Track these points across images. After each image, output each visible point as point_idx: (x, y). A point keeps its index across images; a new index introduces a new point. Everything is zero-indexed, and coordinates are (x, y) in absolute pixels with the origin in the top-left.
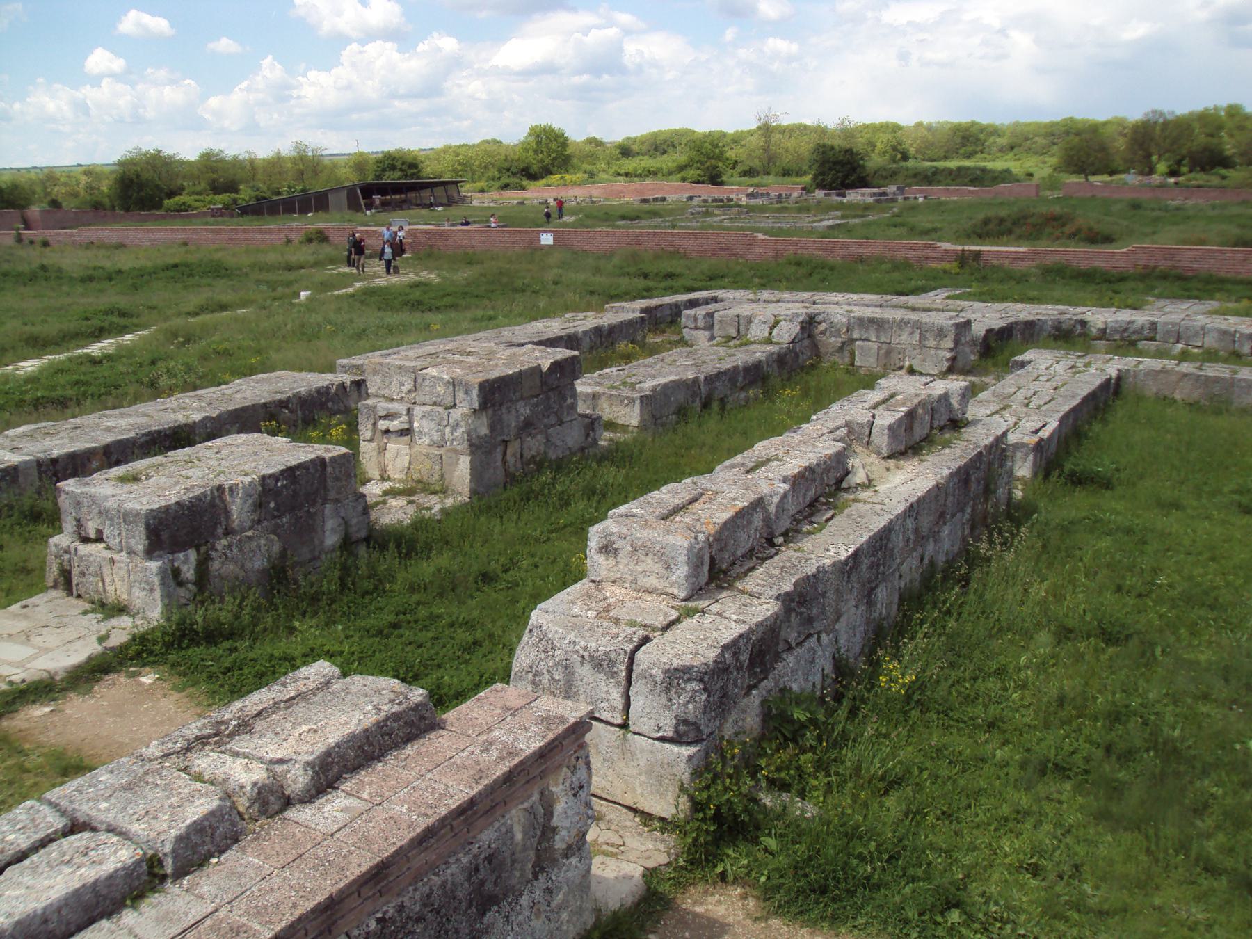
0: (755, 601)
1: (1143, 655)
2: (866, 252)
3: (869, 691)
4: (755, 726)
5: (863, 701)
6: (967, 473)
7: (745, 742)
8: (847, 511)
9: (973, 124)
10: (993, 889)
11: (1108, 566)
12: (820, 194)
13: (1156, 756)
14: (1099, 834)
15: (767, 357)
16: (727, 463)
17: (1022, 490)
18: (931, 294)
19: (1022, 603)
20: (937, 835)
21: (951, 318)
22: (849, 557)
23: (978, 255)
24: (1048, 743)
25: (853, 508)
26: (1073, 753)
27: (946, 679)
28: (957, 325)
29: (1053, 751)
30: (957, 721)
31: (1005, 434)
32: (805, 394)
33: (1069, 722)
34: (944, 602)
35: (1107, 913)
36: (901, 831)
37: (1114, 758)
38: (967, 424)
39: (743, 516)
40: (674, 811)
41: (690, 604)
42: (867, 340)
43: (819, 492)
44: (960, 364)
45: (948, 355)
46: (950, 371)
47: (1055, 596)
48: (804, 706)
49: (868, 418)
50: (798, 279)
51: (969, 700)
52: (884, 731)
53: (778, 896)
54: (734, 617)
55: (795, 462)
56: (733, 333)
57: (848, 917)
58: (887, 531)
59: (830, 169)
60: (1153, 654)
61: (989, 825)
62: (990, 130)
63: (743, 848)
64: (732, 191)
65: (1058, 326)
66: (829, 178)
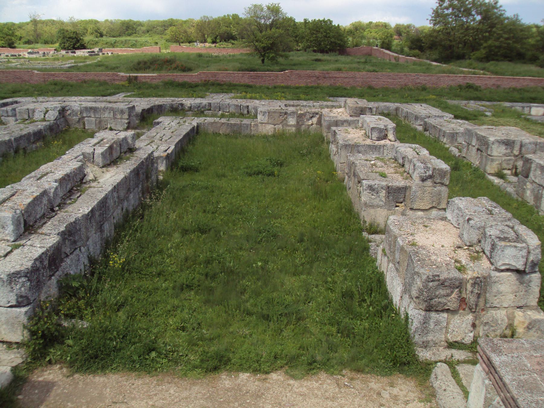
0: (48, 237)
1: (216, 235)
2: (87, 78)
3: (106, 269)
4: (56, 293)
5: (104, 273)
6: (138, 170)
7: (51, 301)
8: (86, 192)
9: (131, 21)
10: (168, 340)
11: (200, 203)
12: (63, 52)
13: (224, 275)
14: (206, 309)
16: (27, 176)
18: (117, 95)
19: (166, 222)
20: (141, 323)
21: (126, 105)
22: (89, 212)
23: (136, 78)
24: (183, 278)
25: (89, 190)
26: (193, 279)
27: (138, 258)
28: (129, 108)
29: (185, 280)
30: (145, 275)
31: (152, 153)
32: (64, 143)
33: (190, 267)
34: (134, 226)
35: (213, 339)
36: (127, 324)
37: (209, 278)
38: (136, 149)
40: (22, 338)
41: (17, 243)
42: (90, 117)
43: (73, 185)
44: (132, 124)
45: (126, 121)
46: (128, 128)
47: (180, 217)
48: (77, 280)
49: (92, 150)
50: (56, 91)
51: (150, 265)
52: (114, 284)
53: (76, 364)
54: (39, 246)
55: (60, 173)
56: (26, 117)
57: (108, 366)
58: (105, 198)
59: (67, 41)
60: (220, 236)
61: (163, 314)
62: (138, 23)
63: (57, 346)
64: (20, 51)
65: (172, 106)
66: (67, 45)
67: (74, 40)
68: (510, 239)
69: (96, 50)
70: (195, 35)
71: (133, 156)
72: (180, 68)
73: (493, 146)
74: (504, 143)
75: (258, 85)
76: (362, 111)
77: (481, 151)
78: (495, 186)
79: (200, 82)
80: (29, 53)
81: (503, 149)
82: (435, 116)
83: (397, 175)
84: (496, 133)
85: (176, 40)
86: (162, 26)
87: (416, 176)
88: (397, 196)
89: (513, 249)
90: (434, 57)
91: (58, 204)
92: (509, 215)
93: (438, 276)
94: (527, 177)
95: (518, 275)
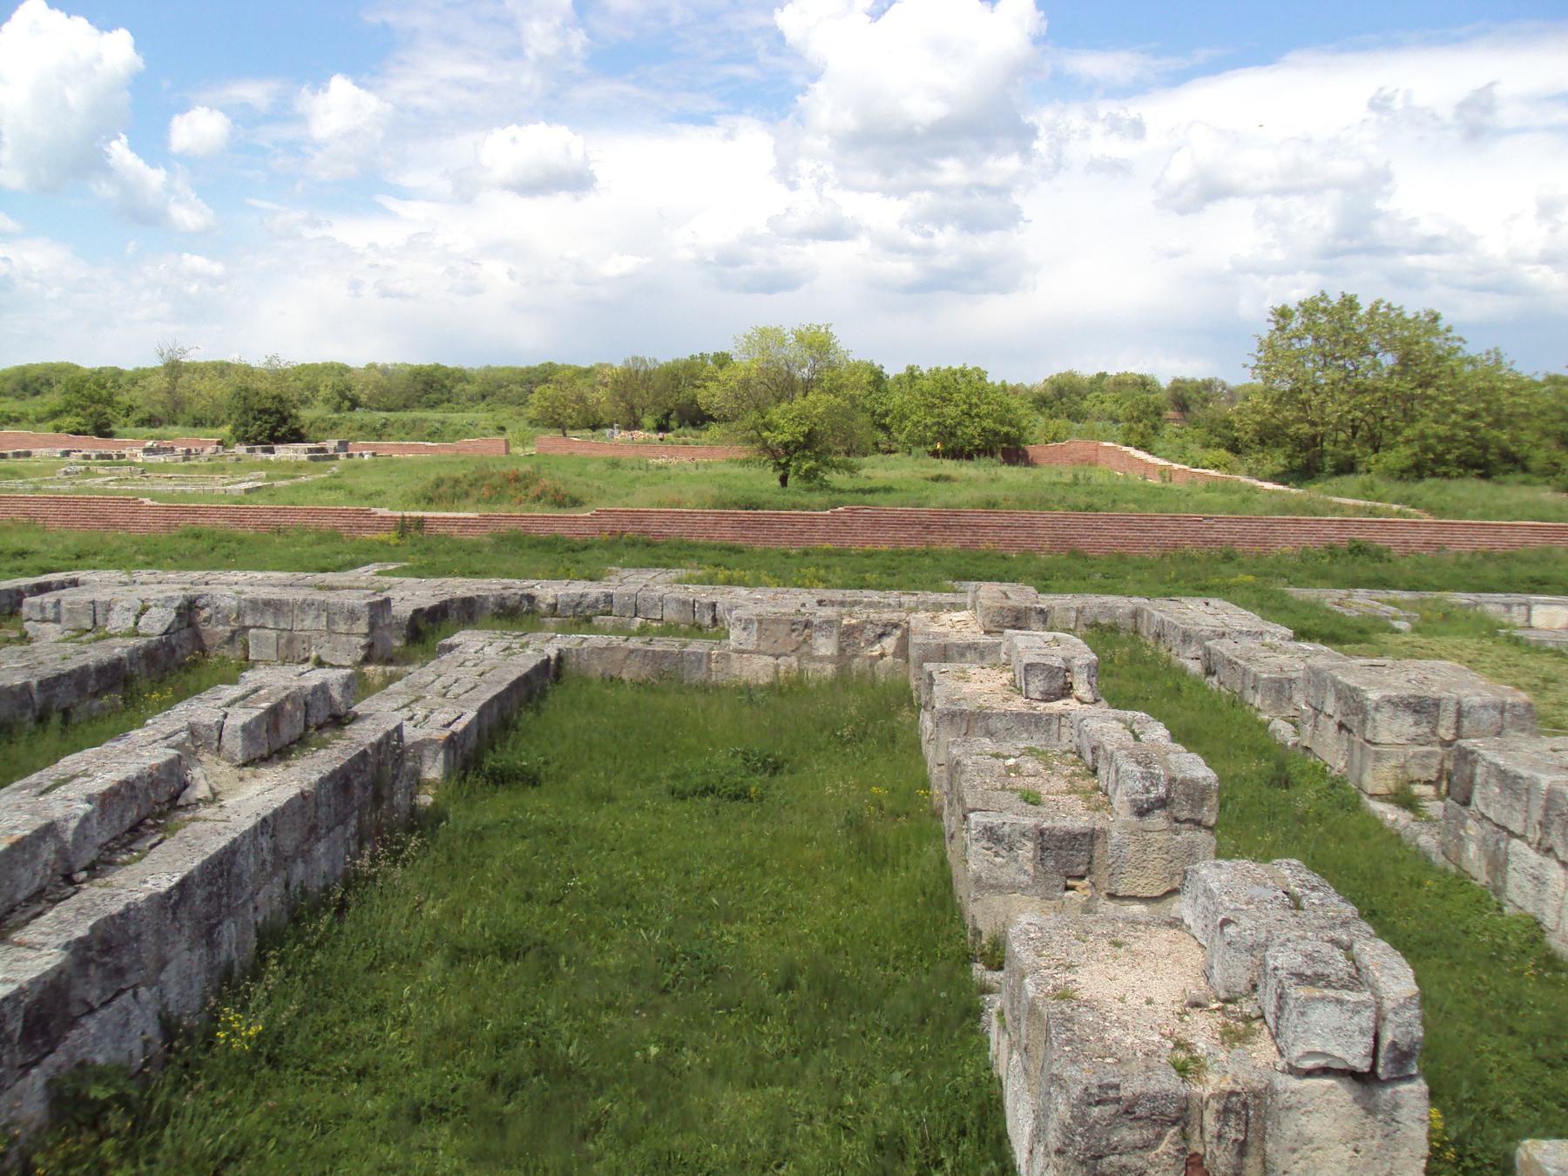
0: (32, 954)
6: (347, 779)
8: (180, 833)
9: (437, 367)
12: (241, 449)
15: (130, 653)
16: (16, 784)
17: (434, 795)
21: (366, 596)
22: (172, 889)
23: (421, 522)
24: (420, 1087)
28: (372, 606)
30: (319, 1074)
38: (355, 718)
39: (24, 848)
42: (263, 627)
43: (143, 813)
44: (378, 651)
45: (363, 642)
51: (335, 1047)
55: (107, 776)
56: (88, 624)
59: (255, 419)
60: (557, 966)
62: (458, 375)
64: (124, 445)
66: (253, 430)
67: (273, 419)
68: (1333, 978)
69: (331, 444)
70: (608, 407)
71: (340, 738)
72: (549, 498)
73: (1378, 716)
74: (1408, 706)
75: (759, 547)
76: (1019, 619)
77: (1350, 731)
78: (1389, 830)
79: (597, 537)
80: (147, 451)
81: (1406, 724)
82: (1240, 633)
83: (1074, 796)
84: (1391, 680)
85: (556, 422)
86: (522, 383)
87: (1120, 800)
88: (1068, 858)
89: (1330, 1008)
90: (1269, 467)
91: (87, 862)
92: (1349, 910)
93: (1117, 1087)
94: (1466, 802)
95: (1356, 1086)
